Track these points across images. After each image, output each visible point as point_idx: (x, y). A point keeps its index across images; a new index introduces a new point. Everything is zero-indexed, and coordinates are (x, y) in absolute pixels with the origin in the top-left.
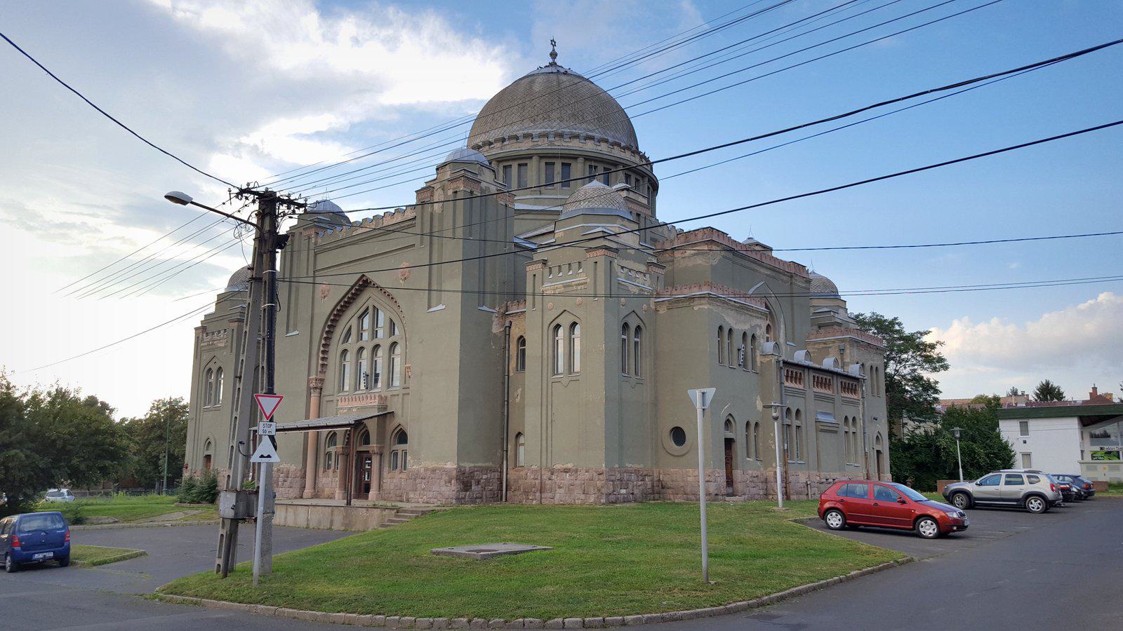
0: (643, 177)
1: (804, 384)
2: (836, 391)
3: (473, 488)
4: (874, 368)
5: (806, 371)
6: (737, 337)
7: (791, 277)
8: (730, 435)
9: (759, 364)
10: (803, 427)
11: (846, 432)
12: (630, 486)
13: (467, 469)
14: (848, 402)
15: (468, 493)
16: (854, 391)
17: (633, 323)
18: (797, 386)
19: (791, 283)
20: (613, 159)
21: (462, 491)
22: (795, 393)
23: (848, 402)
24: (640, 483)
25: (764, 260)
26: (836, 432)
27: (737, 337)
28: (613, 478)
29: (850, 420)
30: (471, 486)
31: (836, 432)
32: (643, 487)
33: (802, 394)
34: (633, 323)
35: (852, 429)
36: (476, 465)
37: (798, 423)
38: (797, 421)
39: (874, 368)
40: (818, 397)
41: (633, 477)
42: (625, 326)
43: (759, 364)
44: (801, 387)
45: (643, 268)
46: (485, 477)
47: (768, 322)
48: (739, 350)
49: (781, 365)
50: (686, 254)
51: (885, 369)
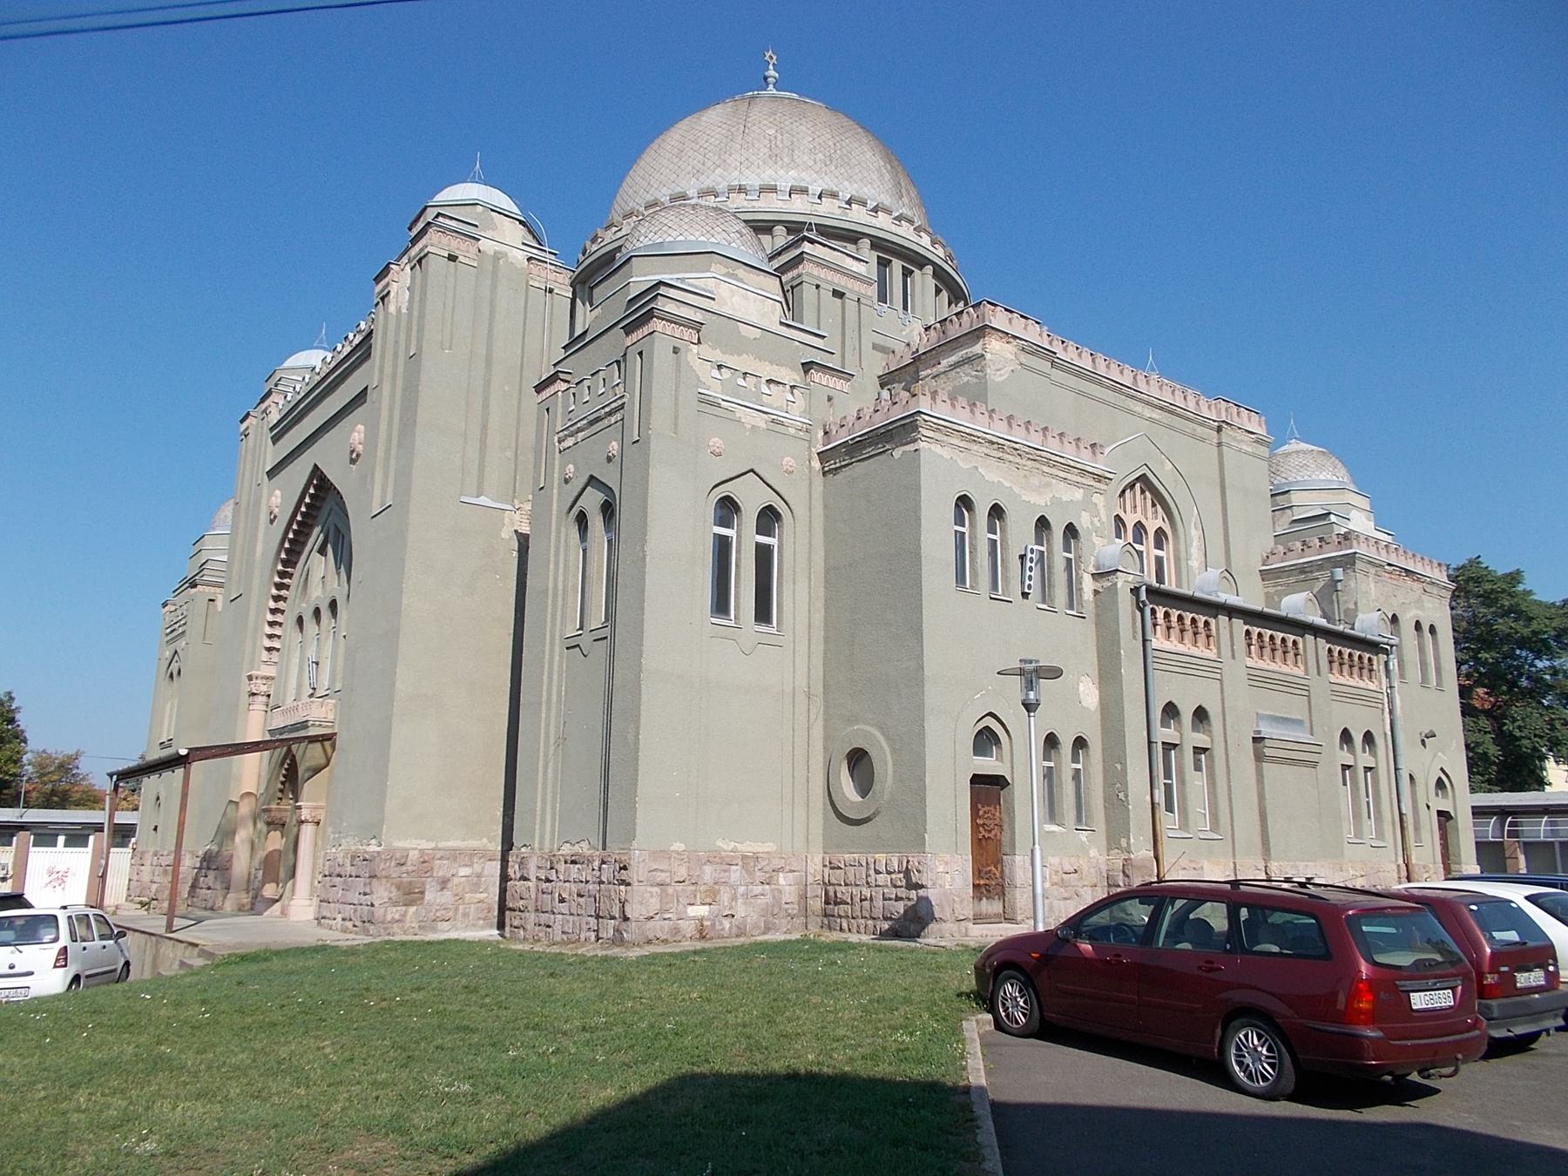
0: (921, 267)
1: (1219, 649)
2: (1313, 670)
3: (428, 896)
4: (1426, 628)
5: (1223, 619)
6: (1020, 533)
7: (1219, 429)
8: (988, 765)
9: (1088, 595)
10: (1219, 753)
11: (1345, 767)
12: (725, 897)
13: (414, 855)
14: (1345, 695)
15: (412, 909)
16: (1367, 670)
17: (751, 499)
18: (1200, 651)
19: (1220, 444)
20: (847, 225)
21: (395, 904)
22: (1188, 666)
23: (1345, 695)
24: (758, 889)
25: (1142, 387)
26: (1314, 764)
27: (1020, 533)
28: (661, 877)
29: (1358, 738)
30: (422, 893)
31: (1314, 764)
32: (768, 899)
33: (1213, 670)
34: (751, 499)
35: (1365, 759)
36: (441, 845)
37: (1201, 739)
38: (1196, 735)
39: (1426, 628)
40: (1257, 679)
41: (736, 873)
42: (728, 509)
43: (1088, 595)
44: (1211, 654)
45: (791, 376)
46: (464, 871)
47: (1159, 523)
48: (1022, 557)
49: (1143, 597)
50: (941, 368)
51: (939, 274)
